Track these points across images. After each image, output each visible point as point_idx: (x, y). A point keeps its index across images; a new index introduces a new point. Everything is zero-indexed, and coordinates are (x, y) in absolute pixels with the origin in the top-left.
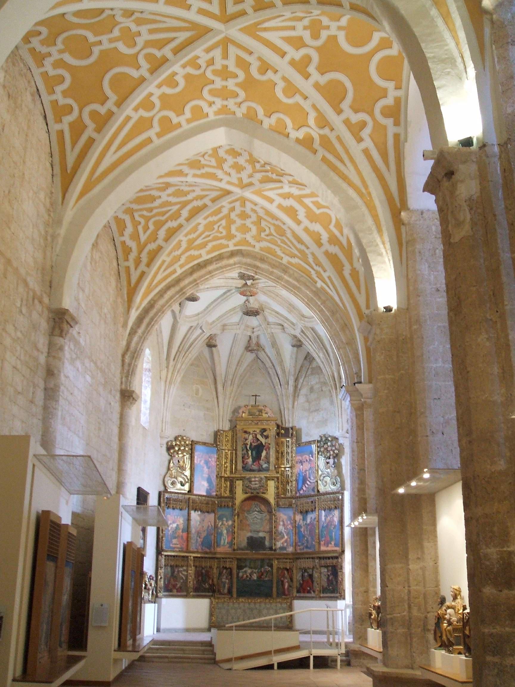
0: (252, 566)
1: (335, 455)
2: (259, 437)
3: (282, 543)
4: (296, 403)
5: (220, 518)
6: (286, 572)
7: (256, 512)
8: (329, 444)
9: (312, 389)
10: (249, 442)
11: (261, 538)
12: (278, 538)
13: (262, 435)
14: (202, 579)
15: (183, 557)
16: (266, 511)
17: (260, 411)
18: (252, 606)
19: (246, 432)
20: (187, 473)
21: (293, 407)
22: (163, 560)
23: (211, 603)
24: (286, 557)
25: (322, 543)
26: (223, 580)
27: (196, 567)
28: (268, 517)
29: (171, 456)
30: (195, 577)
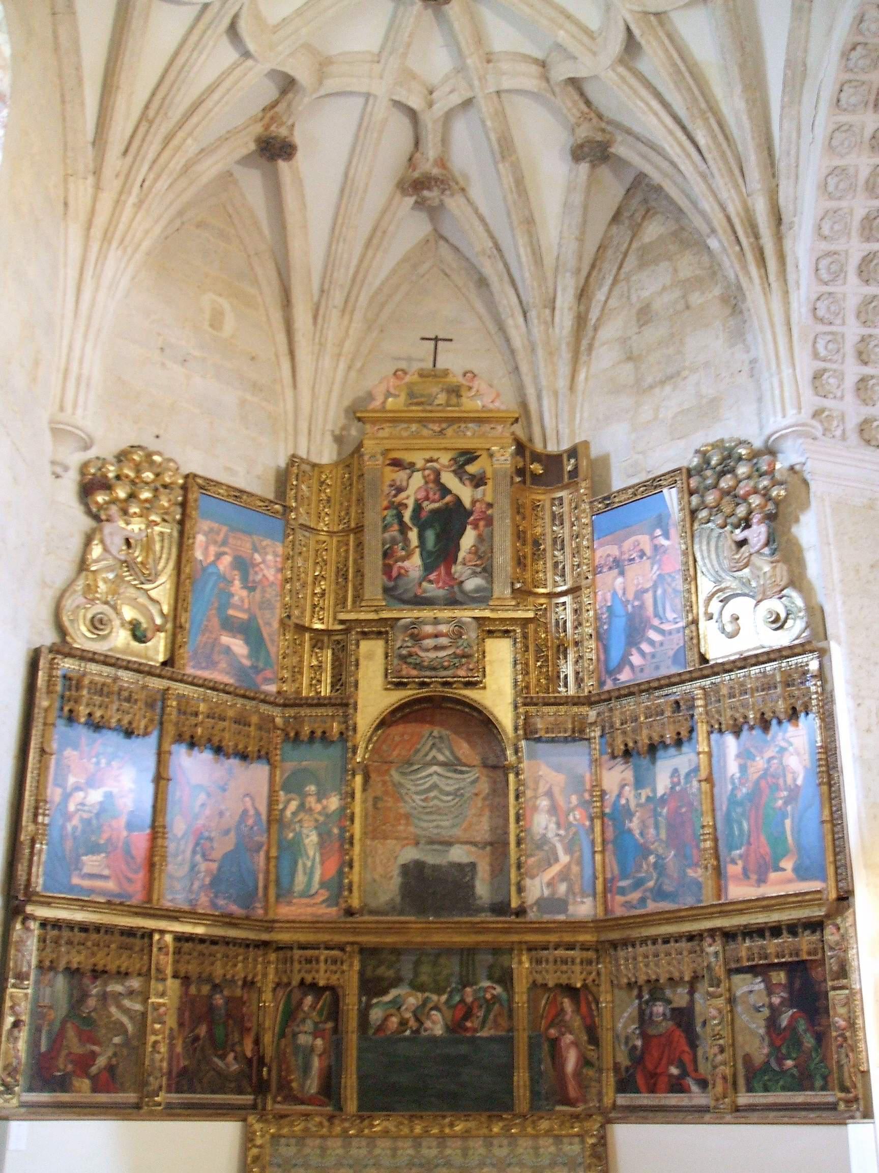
0: (424, 978)
1: (770, 507)
2: (449, 480)
3: (550, 884)
4: (582, 376)
5: (294, 785)
6: (567, 1004)
7: (435, 768)
8: (742, 470)
9: (645, 315)
10: (409, 498)
11: (460, 867)
12: (531, 861)
13: (459, 472)
14: (210, 1031)
15: (130, 932)
16: (476, 760)
17: (455, 391)
18: (430, 1151)
19: (397, 464)
20: (162, 590)
21: (572, 387)
22: (32, 944)
23: (248, 1139)
24: (568, 938)
25: (734, 870)
26: (303, 1039)
27: (186, 980)
28: (484, 786)
29: (96, 518)
30: (181, 1024)
